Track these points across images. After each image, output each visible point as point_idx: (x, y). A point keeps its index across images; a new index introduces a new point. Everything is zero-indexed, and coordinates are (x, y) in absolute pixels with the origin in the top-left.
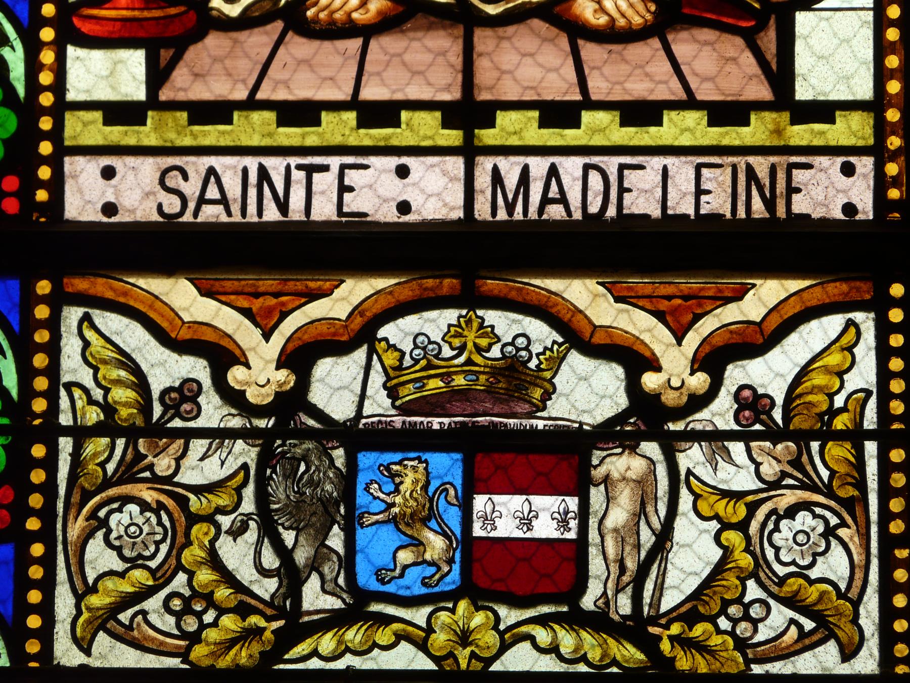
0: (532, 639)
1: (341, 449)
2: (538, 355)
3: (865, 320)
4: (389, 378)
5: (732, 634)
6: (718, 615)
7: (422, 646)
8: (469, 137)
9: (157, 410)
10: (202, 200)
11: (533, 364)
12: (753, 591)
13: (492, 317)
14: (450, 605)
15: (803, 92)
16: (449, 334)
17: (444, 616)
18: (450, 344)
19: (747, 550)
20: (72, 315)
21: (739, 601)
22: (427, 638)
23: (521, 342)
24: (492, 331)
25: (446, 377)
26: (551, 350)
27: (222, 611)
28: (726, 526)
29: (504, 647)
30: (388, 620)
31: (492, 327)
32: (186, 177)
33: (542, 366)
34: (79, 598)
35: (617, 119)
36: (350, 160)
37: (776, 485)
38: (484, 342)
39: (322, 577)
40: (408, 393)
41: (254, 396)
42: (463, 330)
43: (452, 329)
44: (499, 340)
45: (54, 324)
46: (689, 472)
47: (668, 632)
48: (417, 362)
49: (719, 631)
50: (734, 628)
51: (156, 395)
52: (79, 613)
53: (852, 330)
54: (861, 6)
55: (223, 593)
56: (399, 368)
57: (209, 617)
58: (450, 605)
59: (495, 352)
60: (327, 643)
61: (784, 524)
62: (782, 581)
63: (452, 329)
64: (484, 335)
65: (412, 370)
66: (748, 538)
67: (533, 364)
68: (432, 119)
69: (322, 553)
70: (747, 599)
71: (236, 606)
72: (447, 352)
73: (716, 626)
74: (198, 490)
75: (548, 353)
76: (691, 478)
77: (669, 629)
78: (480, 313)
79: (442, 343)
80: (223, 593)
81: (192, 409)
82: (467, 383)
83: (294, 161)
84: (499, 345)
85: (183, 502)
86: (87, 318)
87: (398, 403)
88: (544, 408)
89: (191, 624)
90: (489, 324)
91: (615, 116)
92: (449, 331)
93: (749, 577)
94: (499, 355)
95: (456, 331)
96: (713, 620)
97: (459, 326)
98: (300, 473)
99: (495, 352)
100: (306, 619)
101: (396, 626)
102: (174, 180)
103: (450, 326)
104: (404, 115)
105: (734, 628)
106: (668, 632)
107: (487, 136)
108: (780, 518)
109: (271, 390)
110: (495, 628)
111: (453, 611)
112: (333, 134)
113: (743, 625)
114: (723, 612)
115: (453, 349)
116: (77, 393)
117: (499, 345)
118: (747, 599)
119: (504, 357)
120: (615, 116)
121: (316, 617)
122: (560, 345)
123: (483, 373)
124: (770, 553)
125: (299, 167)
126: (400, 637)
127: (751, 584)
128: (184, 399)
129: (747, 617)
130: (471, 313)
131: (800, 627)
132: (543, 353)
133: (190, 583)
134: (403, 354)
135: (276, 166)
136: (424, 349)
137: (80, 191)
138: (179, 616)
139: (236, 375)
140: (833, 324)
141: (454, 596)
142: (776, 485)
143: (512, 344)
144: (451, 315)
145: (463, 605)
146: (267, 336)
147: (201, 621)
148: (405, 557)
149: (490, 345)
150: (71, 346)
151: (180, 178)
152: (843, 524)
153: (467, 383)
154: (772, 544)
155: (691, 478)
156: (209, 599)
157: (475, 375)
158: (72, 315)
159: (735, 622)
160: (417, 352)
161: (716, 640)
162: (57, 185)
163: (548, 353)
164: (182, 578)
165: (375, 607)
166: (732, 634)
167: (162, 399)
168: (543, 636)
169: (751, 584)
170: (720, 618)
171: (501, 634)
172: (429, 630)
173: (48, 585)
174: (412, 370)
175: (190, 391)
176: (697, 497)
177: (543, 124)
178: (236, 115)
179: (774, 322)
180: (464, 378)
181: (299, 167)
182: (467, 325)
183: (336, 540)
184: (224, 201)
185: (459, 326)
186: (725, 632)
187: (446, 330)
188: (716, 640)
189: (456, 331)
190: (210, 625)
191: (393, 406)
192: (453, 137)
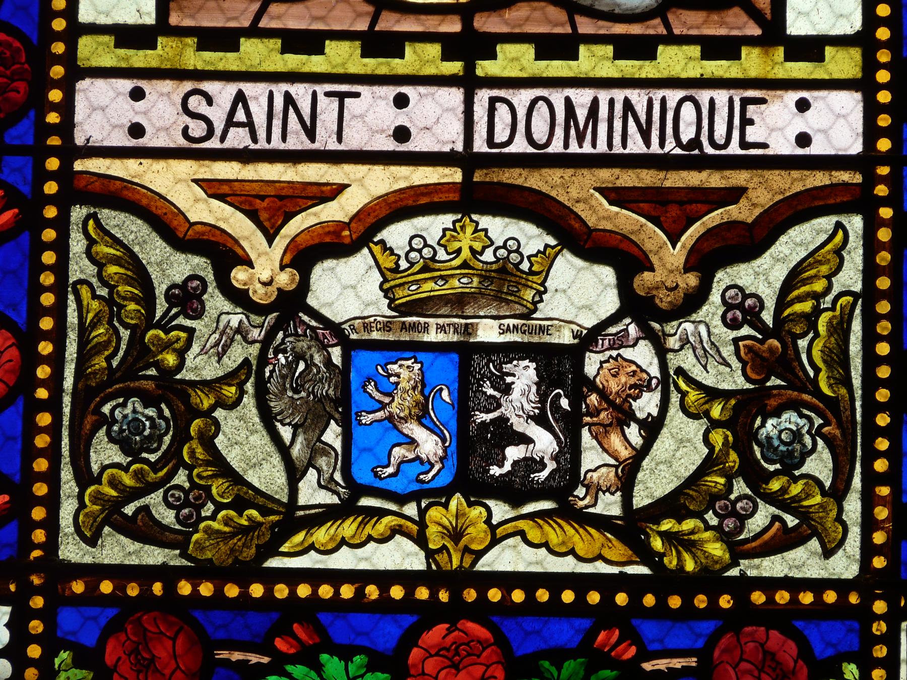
0: (522, 534)
2: (529, 257)
3: (855, 223)
5: (718, 529)
8: (470, 68)
9: (161, 306)
10: (230, 122)
11: (525, 266)
12: (740, 487)
15: (796, 26)
16: (445, 239)
17: (435, 513)
20: (78, 213)
23: (417, 243)
24: (486, 236)
31: (486, 230)
32: (210, 101)
33: (533, 269)
34: (82, 489)
35: (359, 51)
36: (751, 93)
38: (478, 246)
39: (319, 471)
41: (259, 294)
42: (459, 234)
43: (448, 233)
44: (492, 243)
45: (62, 225)
48: (412, 264)
49: (708, 528)
51: (160, 289)
52: (370, 538)
53: (840, 234)
56: (396, 270)
59: (488, 256)
60: (321, 535)
63: (448, 233)
65: (409, 272)
67: (525, 266)
68: (434, 50)
69: (318, 449)
71: (78, 485)
72: (442, 255)
73: (705, 522)
78: (475, 217)
79: (437, 247)
82: (461, 285)
83: (321, 89)
84: (492, 249)
86: (94, 216)
88: (535, 310)
90: (484, 227)
91: (695, 51)
92: (444, 235)
96: (699, 515)
97: (455, 230)
99: (488, 256)
100: (301, 513)
102: (195, 103)
103: (445, 230)
104: (829, 51)
107: (484, 68)
109: (273, 291)
111: (446, 506)
112: (212, 63)
114: (711, 506)
115: (448, 254)
116: (85, 292)
119: (498, 260)
120: (355, 49)
121: (313, 511)
122: (553, 247)
125: (328, 94)
126: (396, 531)
131: (783, 522)
132: (536, 255)
133: (190, 478)
134: (399, 257)
135: (301, 92)
137: (850, 125)
139: (239, 275)
140: (826, 223)
141: (446, 493)
143: (504, 246)
144: (447, 220)
145: (456, 501)
150: (77, 244)
151: (204, 102)
152: (827, 423)
153: (461, 285)
158: (78, 213)
160: (413, 255)
162: (67, 108)
165: (365, 502)
166: (718, 529)
167: (168, 296)
172: (422, 524)
173: (53, 478)
174: (409, 272)
176: (684, 394)
177: (539, 57)
178: (744, 51)
180: (459, 280)
181: (328, 94)
182: (462, 230)
183: (332, 435)
184: (250, 124)
185: (455, 230)
186: (712, 528)
190: (207, 518)
192: (455, 67)
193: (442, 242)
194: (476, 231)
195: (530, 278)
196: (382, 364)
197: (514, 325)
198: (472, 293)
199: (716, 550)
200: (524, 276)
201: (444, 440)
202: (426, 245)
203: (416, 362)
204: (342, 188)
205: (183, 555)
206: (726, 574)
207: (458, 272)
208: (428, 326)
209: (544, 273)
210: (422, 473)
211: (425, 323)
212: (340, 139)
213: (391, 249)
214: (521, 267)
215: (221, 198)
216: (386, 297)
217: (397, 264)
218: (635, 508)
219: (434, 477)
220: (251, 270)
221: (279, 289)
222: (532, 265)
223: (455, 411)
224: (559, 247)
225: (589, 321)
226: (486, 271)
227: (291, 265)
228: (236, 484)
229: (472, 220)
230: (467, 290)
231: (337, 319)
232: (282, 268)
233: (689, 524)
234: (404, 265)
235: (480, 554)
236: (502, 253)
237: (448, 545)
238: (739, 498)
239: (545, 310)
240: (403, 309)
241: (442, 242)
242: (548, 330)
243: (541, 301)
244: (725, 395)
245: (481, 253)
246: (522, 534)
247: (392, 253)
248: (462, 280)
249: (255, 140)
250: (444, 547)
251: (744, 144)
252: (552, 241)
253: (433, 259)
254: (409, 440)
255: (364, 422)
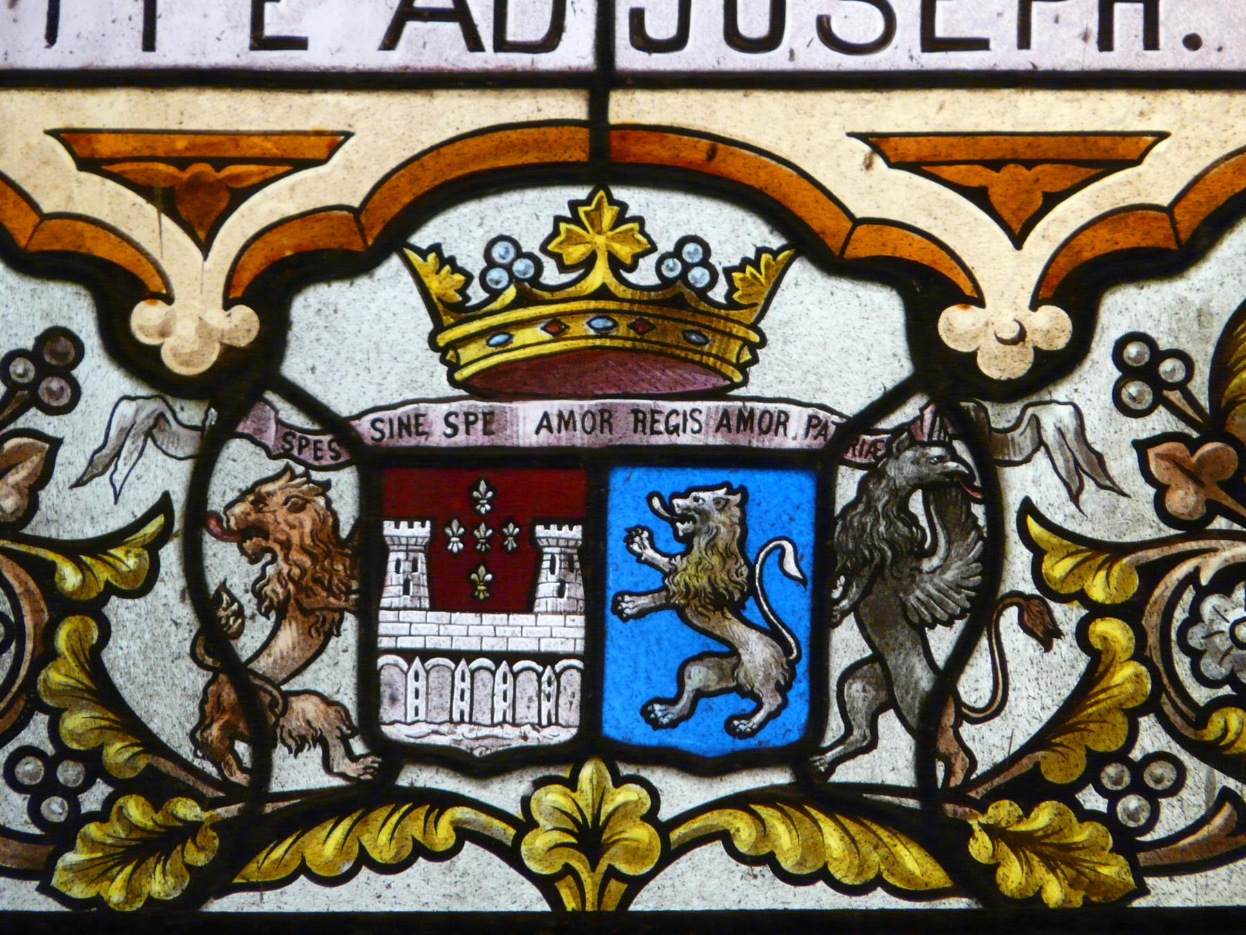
0: (726, 837)
1: (348, 470)
4: (439, 328)
5: (1108, 819)
6: (1080, 785)
7: (511, 855)
11: (719, 293)
13: (636, 199)
14: (565, 773)
16: (558, 240)
18: (558, 258)
19: (1139, 655)
21: (1121, 756)
22: (518, 840)
24: (642, 232)
25: (556, 326)
26: (755, 263)
27: (122, 788)
28: (1098, 611)
29: (669, 855)
30: (441, 801)
31: (640, 220)
37: (1194, 528)
38: (624, 252)
40: (476, 358)
44: (653, 248)
46: (1028, 508)
47: (983, 820)
48: (494, 294)
50: (1112, 807)
54: (969, 264)
55: (117, 752)
57: (92, 800)
58: (565, 773)
59: (645, 275)
61: (1210, 604)
62: (1202, 715)
64: (626, 238)
66: (1140, 636)
70: (1136, 754)
74: (74, 550)
75: (749, 269)
76: (1031, 522)
77: (984, 811)
78: (620, 193)
80: (117, 752)
81: (62, 389)
84: (652, 259)
85: (44, 574)
87: (459, 376)
89: (55, 808)
92: (556, 233)
93: (1143, 710)
94: (654, 280)
95: (568, 231)
96: (1066, 795)
98: (12, 427)
101: (460, 813)
103: (558, 220)
105: (1112, 807)
106: (983, 820)
108: (1202, 594)
110: (651, 817)
111: (572, 784)
113: (1132, 802)
114: (1091, 777)
117: (654, 257)
118: (1136, 754)
123: (620, 312)
124: (1182, 665)
126: (464, 834)
127: (1147, 723)
128: (44, 371)
129: (1137, 787)
130: (601, 193)
132: (741, 268)
134: (469, 278)
136: (508, 268)
138: (37, 794)
142: (1194, 528)
143: (677, 253)
144: (557, 199)
146: (205, 247)
147: (75, 806)
148: (697, 676)
149: (636, 258)
154: (1187, 649)
155: (1031, 522)
156: (94, 765)
157: (609, 319)
159: (1113, 798)
160: (495, 274)
161: (1083, 834)
163: (749, 269)
164: (40, 722)
168: (744, 832)
169: (1147, 723)
170: (1086, 791)
171: (664, 829)
175: (54, 354)
179: (1201, 205)
180: (589, 324)
185: (576, 220)
187: (549, 229)
188: (1083, 834)
189: (568, 231)
190: (93, 817)
191: (453, 382)
193: (550, 247)
194: (620, 219)
195: (733, 314)
196: (666, 494)
197: (560, 415)
198: (623, 349)
199: (1114, 870)
200: (723, 312)
201: (787, 650)
202: (520, 255)
203: (731, 491)
204: (336, 140)
205: (46, 889)
206: (67, 910)
207: (593, 304)
208: (611, 416)
209: (759, 309)
210: (739, 717)
211: (781, 412)
212: (149, 42)
213: (451, 261)
214: (710, 294)
215: (916, 167)
216: (443, 360)
217: (462, 291)
218: (1091, 785)
219: (762, 725)
220: (168, 308)
221: (1036, 350)
222: (732, 289)
223: (808, 593)
224: (409, 252)
225: (852, 405)
226: (640, 302)
227: (1057, 300)
228: (146, 751)
229: (612, 202)
230: (608, 343)
231: (343, 407)
232: (1035, 305)
233: (1044, 816)
234: (477, 294)
235: (636, 884)
236: (673, 269)
237: (578, 866)
238: (1150, 758)
239: (762, 381)
240: (477, 383)
241: (550, 247)
242: (418, 425)
243: (755, 360)
244: (1113, 551)
245: (632, 268)
246: (726, 837)
247: (456, 269)
248: (594, 323)
249: (474, 43)
250: (568, 870)
251: (930, 42)
252: (776, 242)
253: (535, 280)
254: (725, 649)
255: (628, 611)
